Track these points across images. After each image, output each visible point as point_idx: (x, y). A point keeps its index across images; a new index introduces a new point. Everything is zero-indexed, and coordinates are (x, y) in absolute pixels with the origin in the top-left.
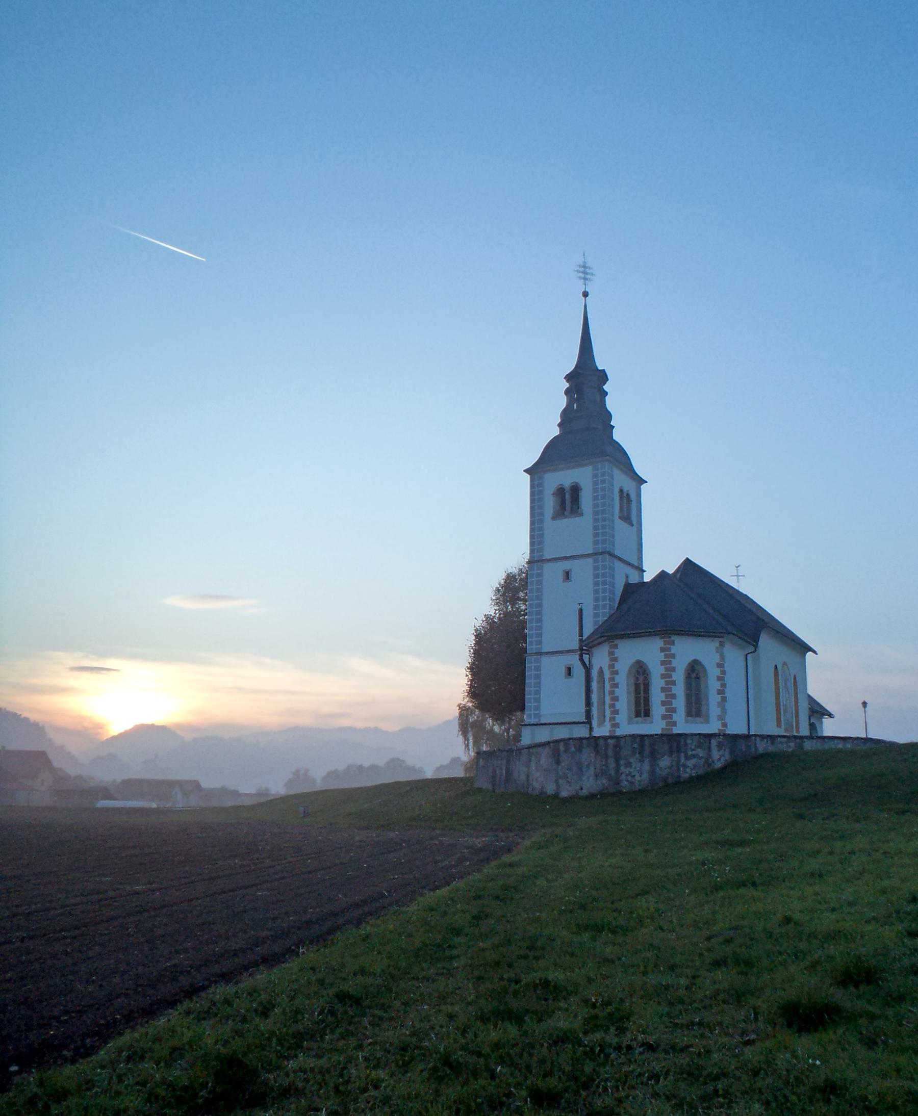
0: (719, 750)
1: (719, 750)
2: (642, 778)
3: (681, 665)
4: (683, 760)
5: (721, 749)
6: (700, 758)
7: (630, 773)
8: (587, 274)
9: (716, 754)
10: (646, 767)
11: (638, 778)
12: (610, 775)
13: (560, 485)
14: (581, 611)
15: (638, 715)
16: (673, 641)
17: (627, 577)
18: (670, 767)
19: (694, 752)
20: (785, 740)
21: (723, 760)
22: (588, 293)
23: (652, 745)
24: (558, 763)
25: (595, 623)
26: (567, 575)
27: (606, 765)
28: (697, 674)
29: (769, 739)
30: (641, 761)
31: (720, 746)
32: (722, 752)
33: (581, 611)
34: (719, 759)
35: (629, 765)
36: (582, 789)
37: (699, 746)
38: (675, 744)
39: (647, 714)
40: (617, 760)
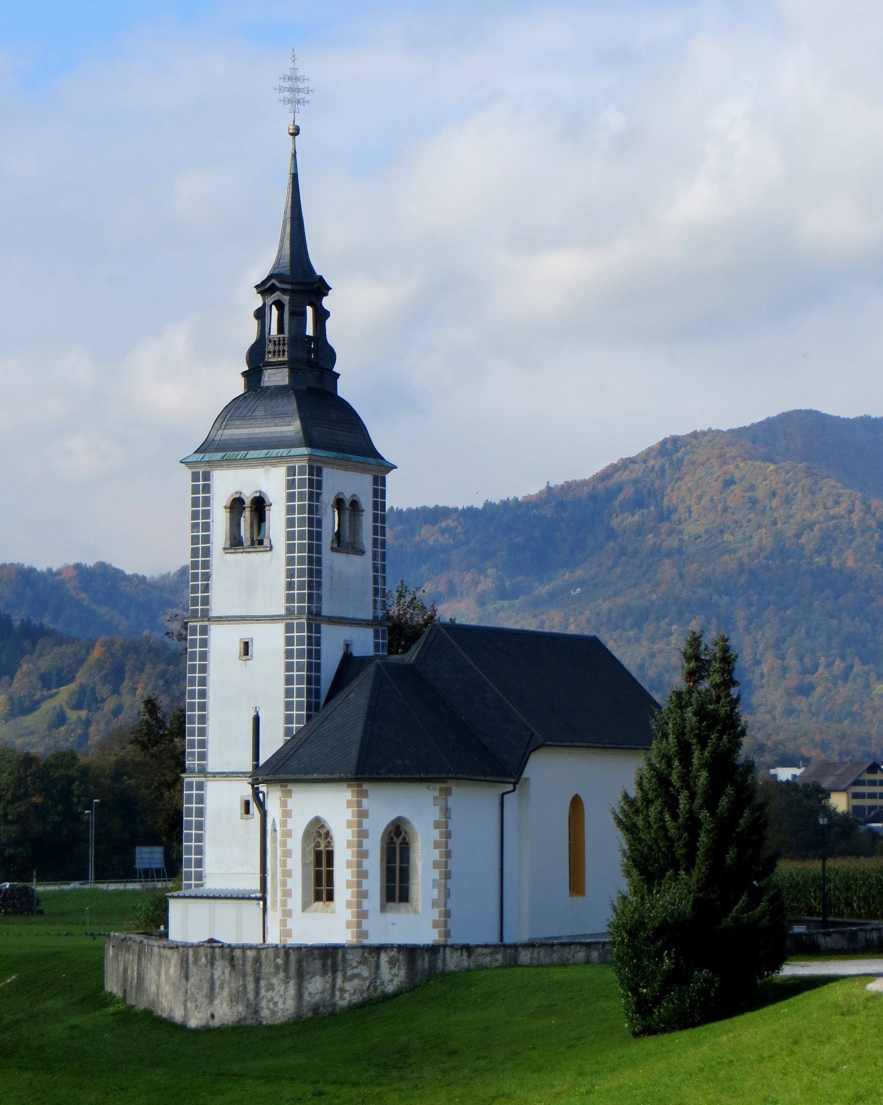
0: (391, 969)
1: (391, 969)
2: (287, 1005)
3: (378, 825)
4: (339, 981)
5: (394, 967)
6: (364, 979)
7: (272, 998)
8: (298, 90)
9: (385, 971)
10: (292, 990)
11: (280, 1005)
12: (248, 1000)
13: (236, 493)
14: (257, 720)
15: (318, 897)
16: (367, 791)
17: (347, 646)
18: (323, 992)
19: (356, 971)
20: (488, 951)
21: (396, 981)
22: (298, 127)
23: (299, 961)
24: (187, 978)
25: (288, 731)
26: (246, 648)
27: (245, 987)
28: (404, 839)
29: (464, 951)
30: (286, 982)
31: (392, 962)
32: (395, 971)
33: (257, 720)
34: (392, 980)
35: (270, 987)
36: (213, 1016)
37: (363, 962)
38: (329, 962)
39: (330, 897)
40: (257, 980)
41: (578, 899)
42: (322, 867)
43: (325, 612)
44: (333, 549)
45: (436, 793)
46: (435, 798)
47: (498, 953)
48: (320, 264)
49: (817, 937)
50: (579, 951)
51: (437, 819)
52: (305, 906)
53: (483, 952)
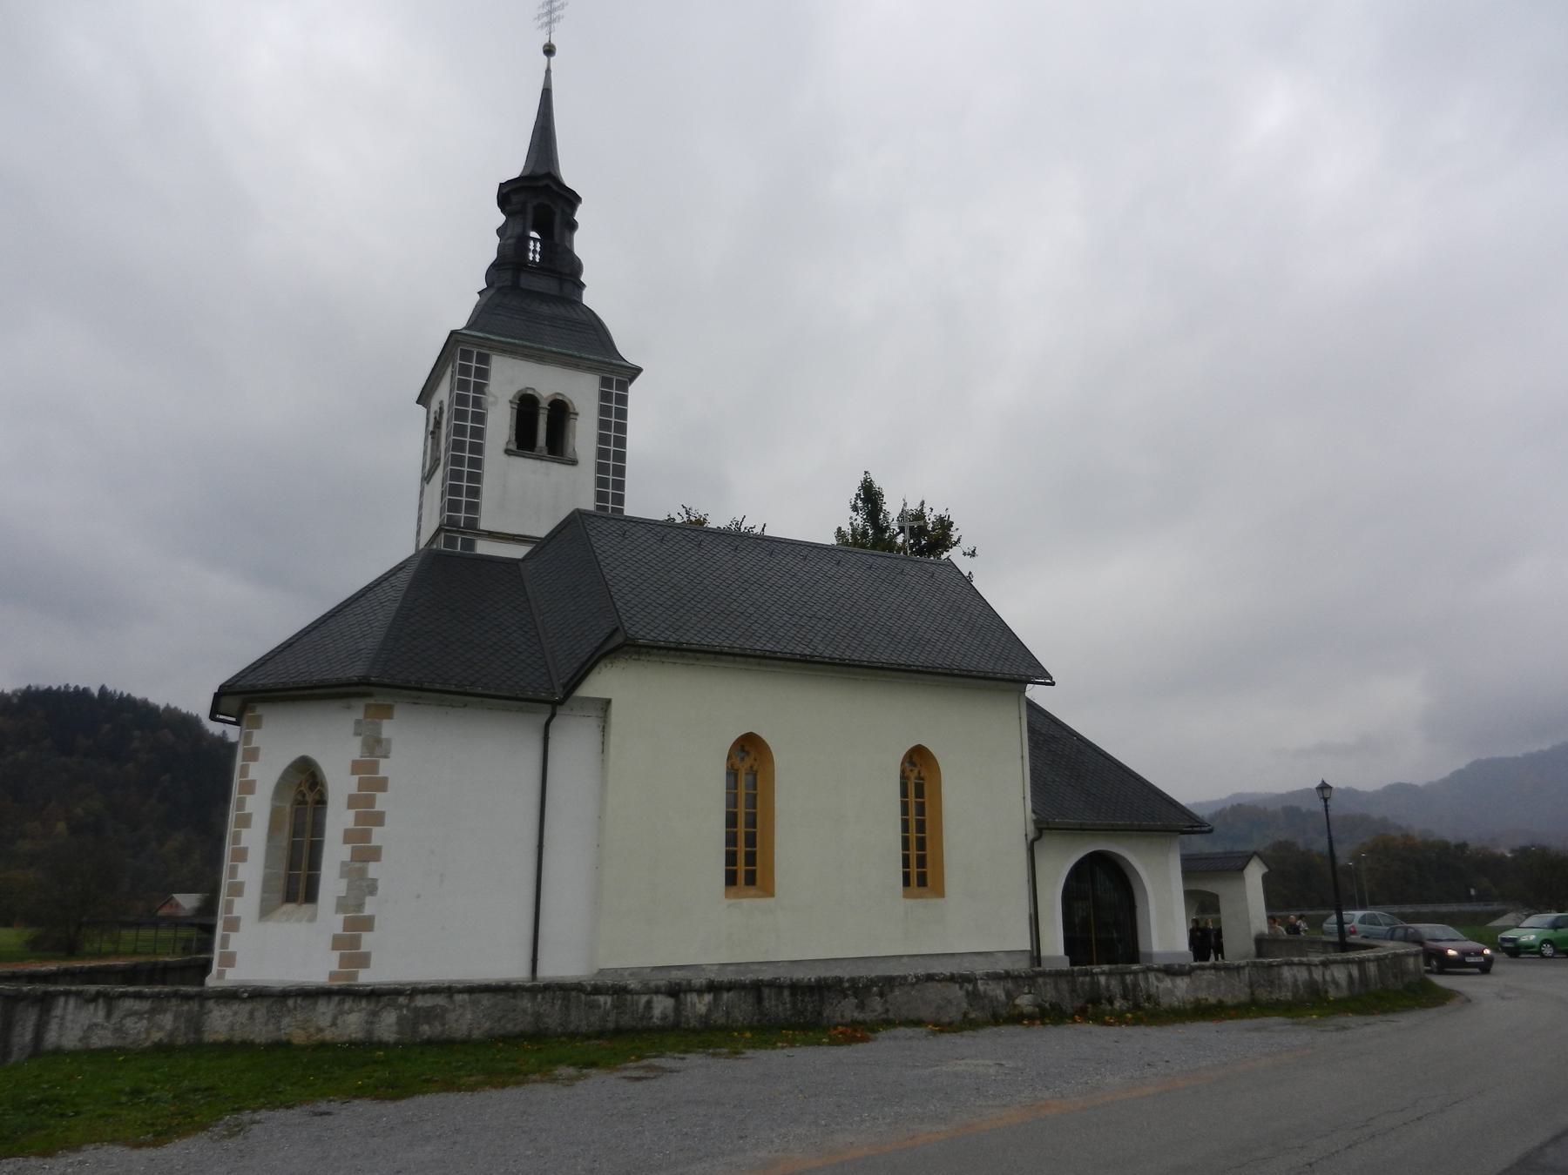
15: (290, 897)
39: (311, 896)
41: (750, 905)
42: (918, 872)
43: (485, 524)
44: (508, 452)
45: (359, 714)
46: (358, 722)
47: (164, 1011)
48: (570, 175)
49: (1147, 979)
50: (351, 1011)
51: (357, 757)
52: (265, 912)
53: (136, 1008)
